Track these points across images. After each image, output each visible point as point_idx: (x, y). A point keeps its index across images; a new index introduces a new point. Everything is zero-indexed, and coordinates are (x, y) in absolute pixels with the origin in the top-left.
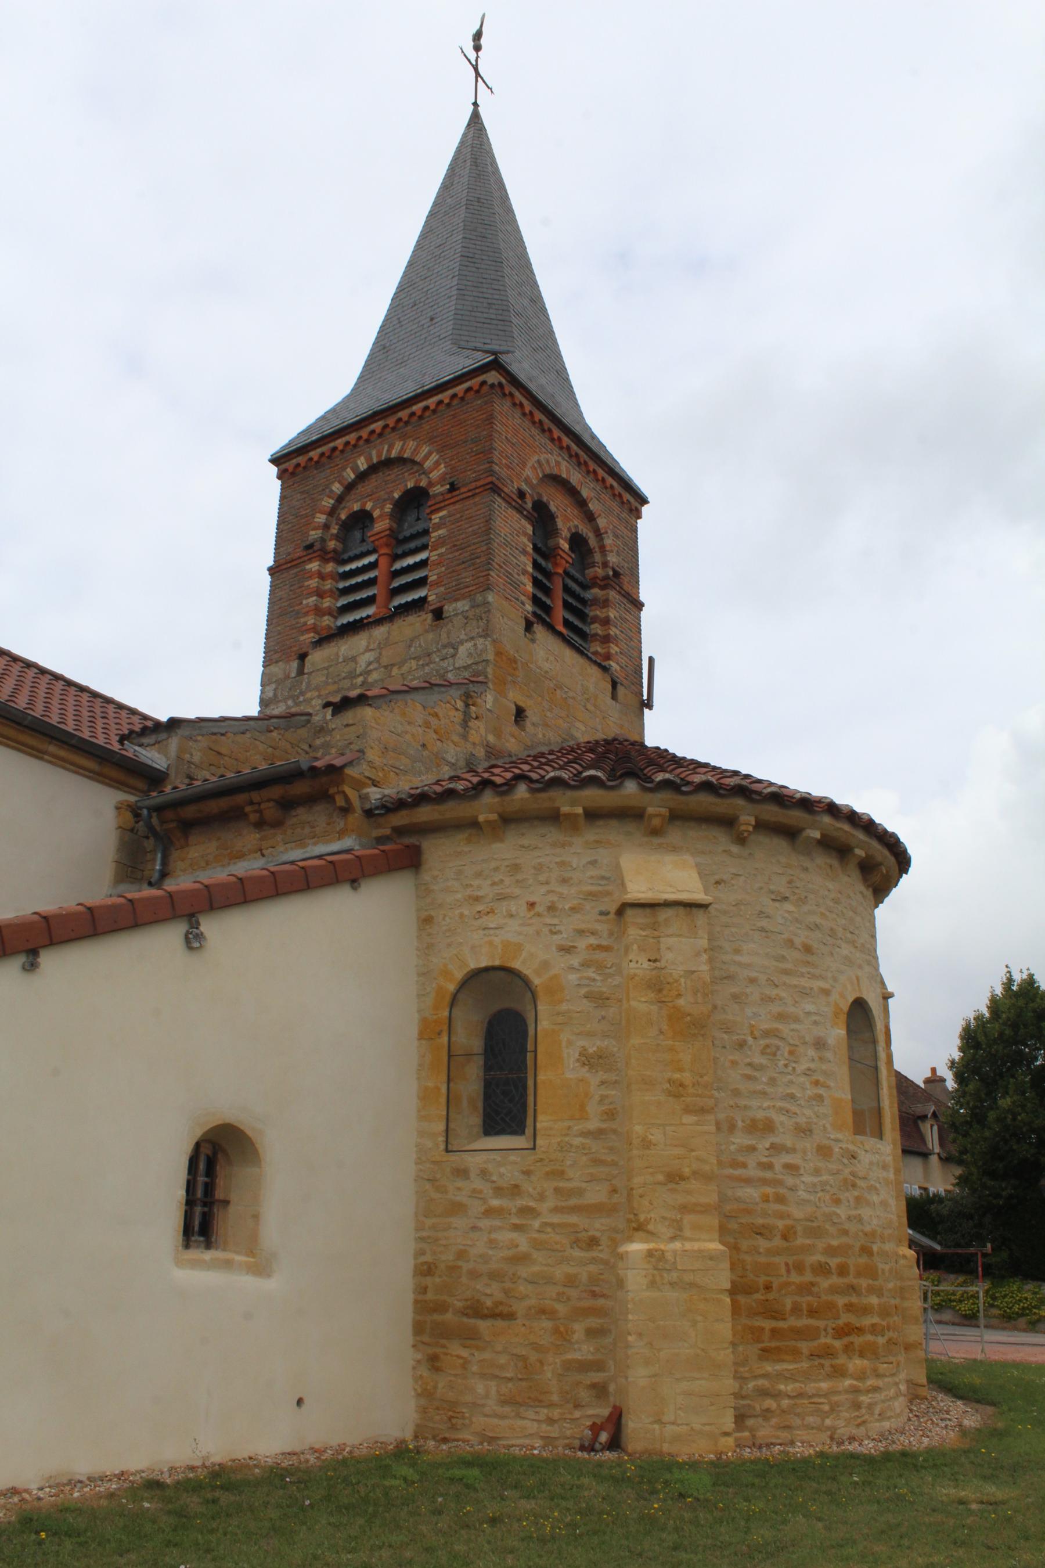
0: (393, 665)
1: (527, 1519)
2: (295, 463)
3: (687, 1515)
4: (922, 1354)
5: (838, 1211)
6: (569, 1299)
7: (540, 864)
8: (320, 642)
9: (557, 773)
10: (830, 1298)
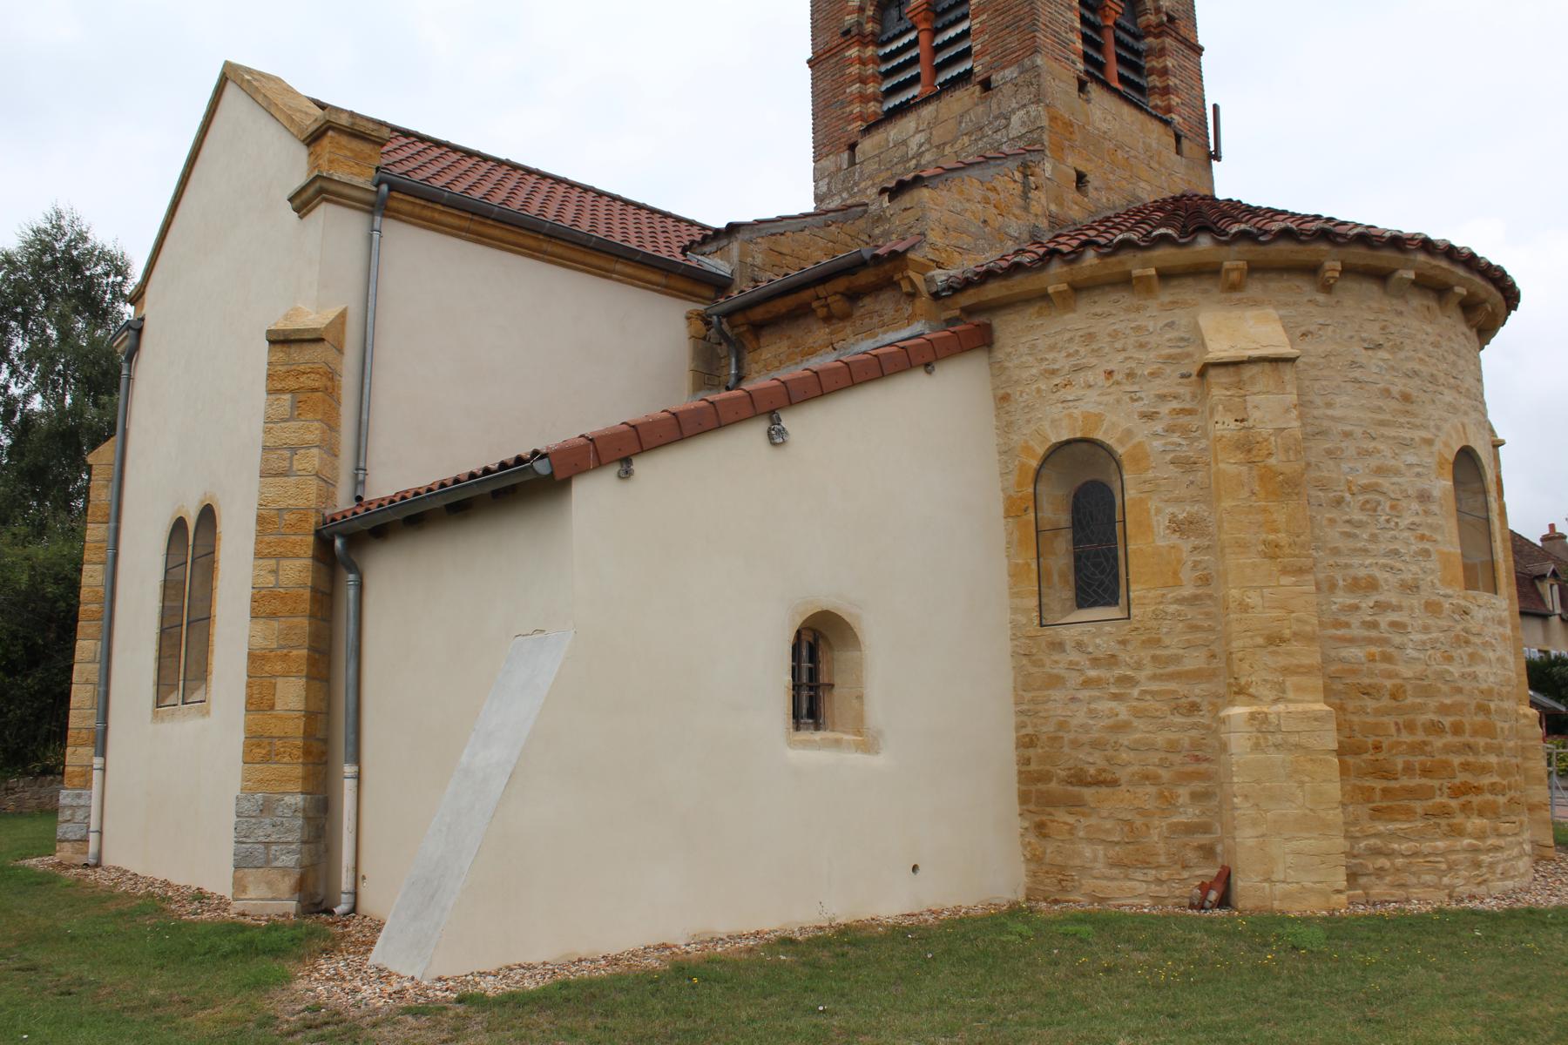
0: (945, 144)
8: (867, 131)
10: (1444, 757)
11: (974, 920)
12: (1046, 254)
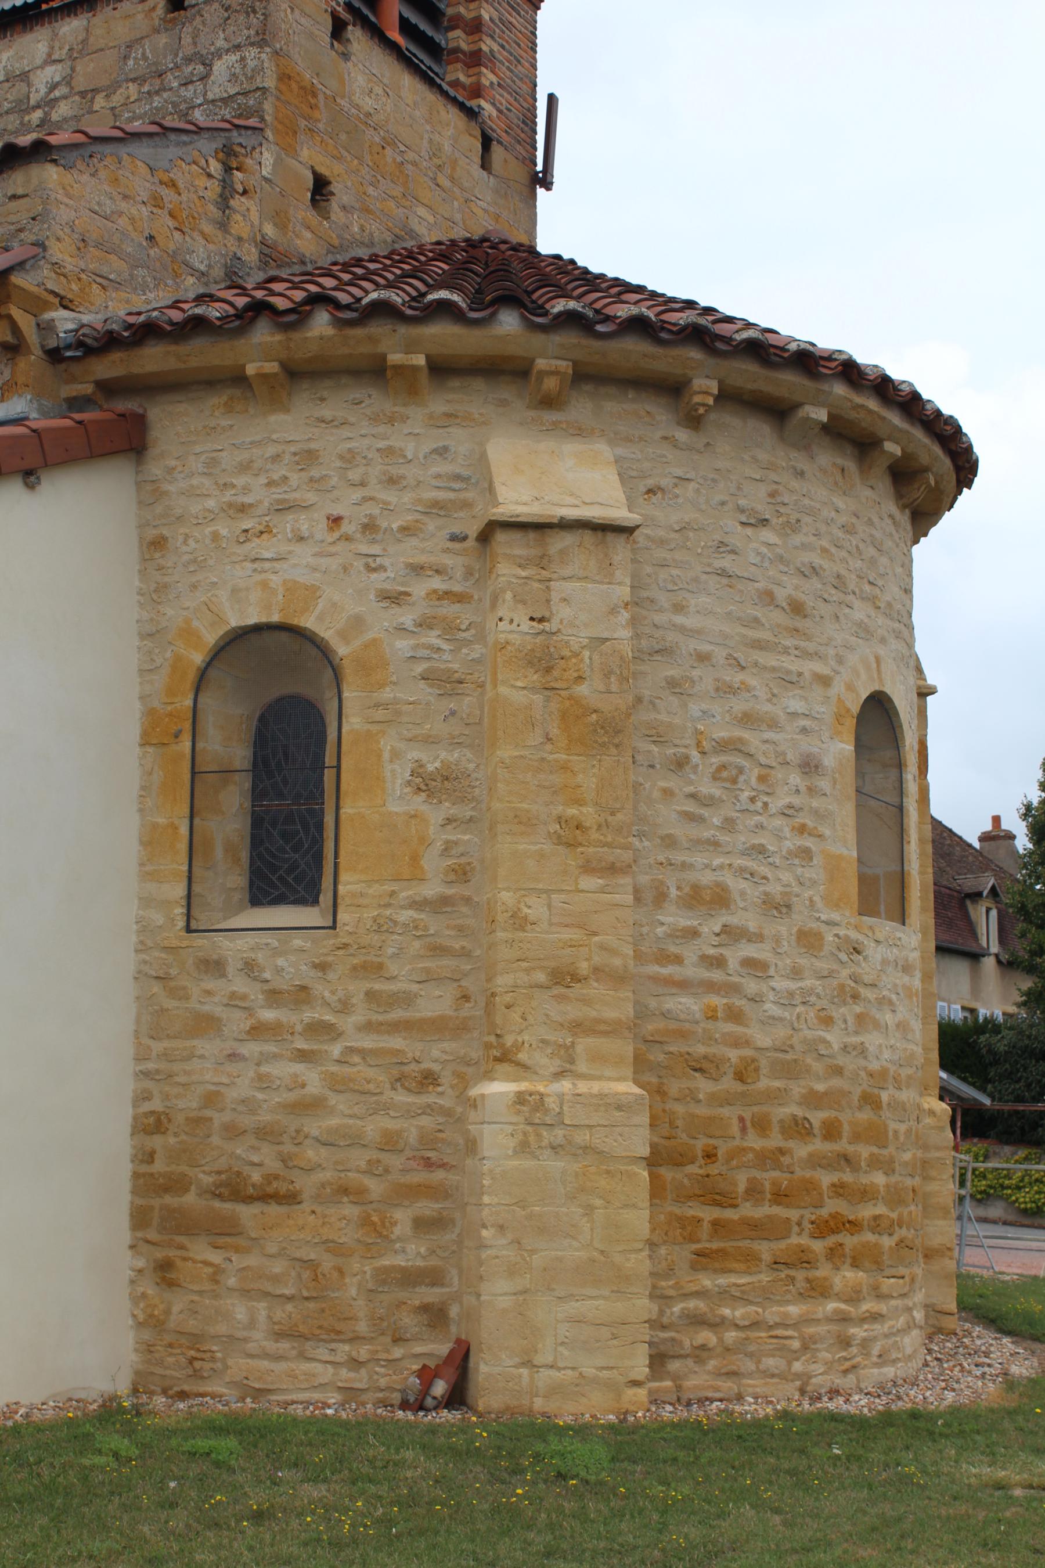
0: (95, 91)
1: (313, 1513)
3: (568, 1506)
4: (951, 1265)
5: (828, 1037)
6: (387, 1171)
7: (350, 450)
9: (384, 294)
10: (808, 1174)
11: (39, 1429)
12: (248, 308)
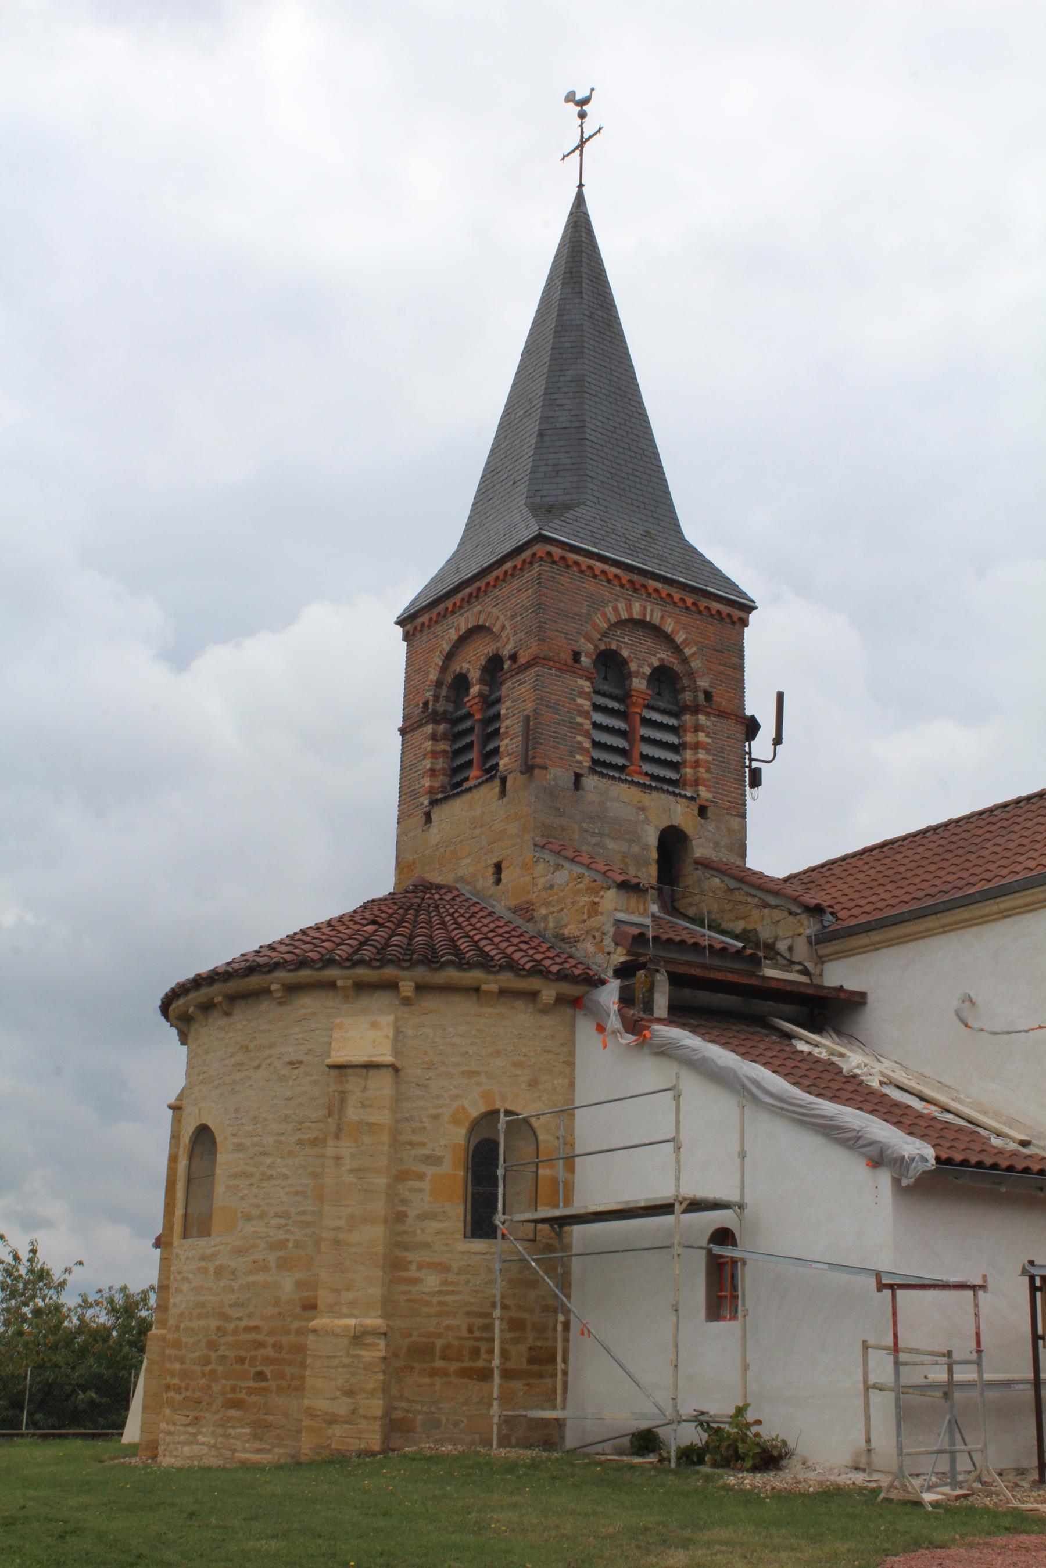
2: (414, 623)
